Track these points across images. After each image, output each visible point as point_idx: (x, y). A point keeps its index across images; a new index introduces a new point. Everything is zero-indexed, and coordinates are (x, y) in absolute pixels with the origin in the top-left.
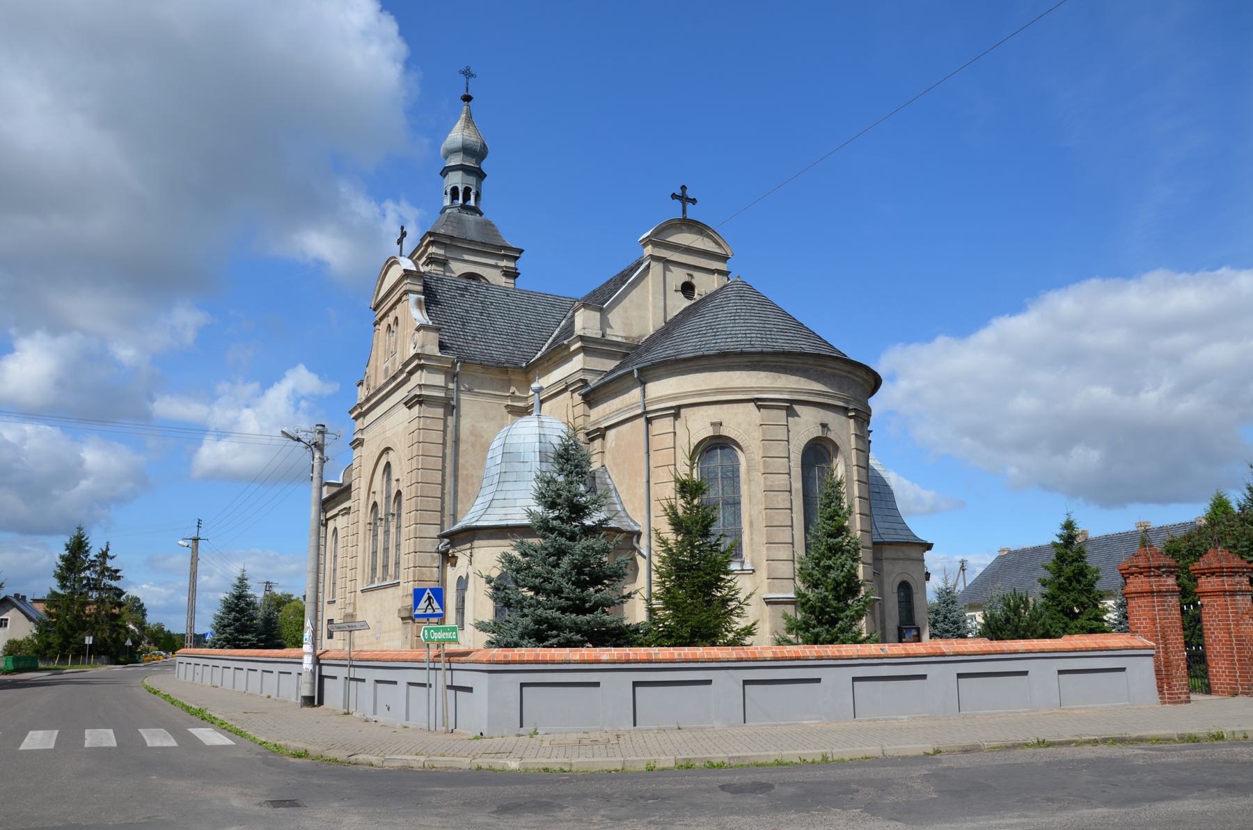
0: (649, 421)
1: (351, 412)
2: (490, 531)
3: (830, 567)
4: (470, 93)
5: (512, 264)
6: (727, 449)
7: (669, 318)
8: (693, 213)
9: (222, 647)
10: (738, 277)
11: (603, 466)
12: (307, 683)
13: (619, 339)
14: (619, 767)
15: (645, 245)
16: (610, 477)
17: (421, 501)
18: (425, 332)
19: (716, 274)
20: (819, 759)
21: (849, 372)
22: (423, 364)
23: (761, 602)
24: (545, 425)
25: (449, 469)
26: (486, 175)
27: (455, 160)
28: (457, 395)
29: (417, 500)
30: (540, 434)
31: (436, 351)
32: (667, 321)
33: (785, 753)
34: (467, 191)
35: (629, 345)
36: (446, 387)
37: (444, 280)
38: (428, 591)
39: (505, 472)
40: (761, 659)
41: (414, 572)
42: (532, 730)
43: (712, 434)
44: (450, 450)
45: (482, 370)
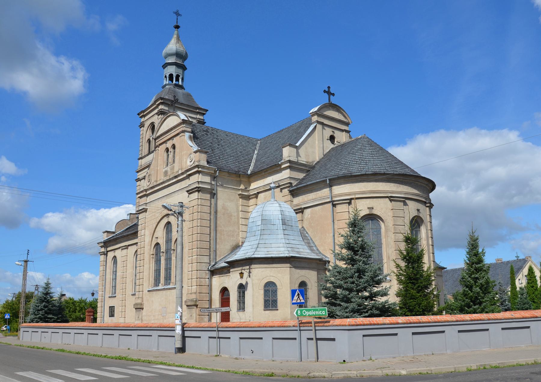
0: (334, 206)
1: (137, 194)
2: (261, 260)
3: (477, 278)
4: (178, 24)
5: (201, 117)
6: (374, 221)
7: (325, 153)
8: (334, 100)
9: (37, 322)
10: (365, 135)
11: (302, 227)
12: (179, 340)
13: (304, 163)
14: (453, 370)
15: (313, 115)
16: (307, 233)
17: (200, 243)
18: (200, 154)
19: (344, 132)
20: (533, 362)
21: (427, 185)
22: (200, 171)
23: (394, 296)
24: (282, 205)
25: (212, 227)
26: (187, 69)
27: (172, 60)
28: (216, 188)
29: (197, 243)
30: (281, 210)
31: (205, 164)
32: (324, 154)
33: (520, 360)
34: (178, 77)
35: (310, 166)
36: (211, 183)
37: (196, 126)
38: (298, 291)
39: (264, 230)
40: (451, 321)
41: (197, 281)
42: (369, 357)
43: (368, 213)
44: (213, 217)
45: (228, 175)
